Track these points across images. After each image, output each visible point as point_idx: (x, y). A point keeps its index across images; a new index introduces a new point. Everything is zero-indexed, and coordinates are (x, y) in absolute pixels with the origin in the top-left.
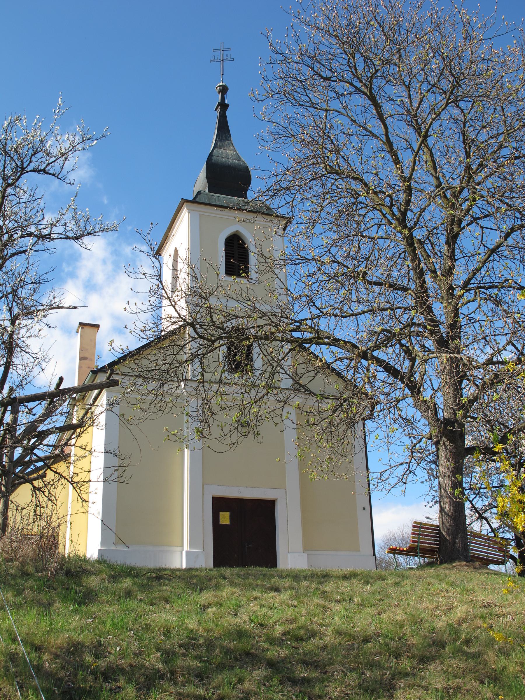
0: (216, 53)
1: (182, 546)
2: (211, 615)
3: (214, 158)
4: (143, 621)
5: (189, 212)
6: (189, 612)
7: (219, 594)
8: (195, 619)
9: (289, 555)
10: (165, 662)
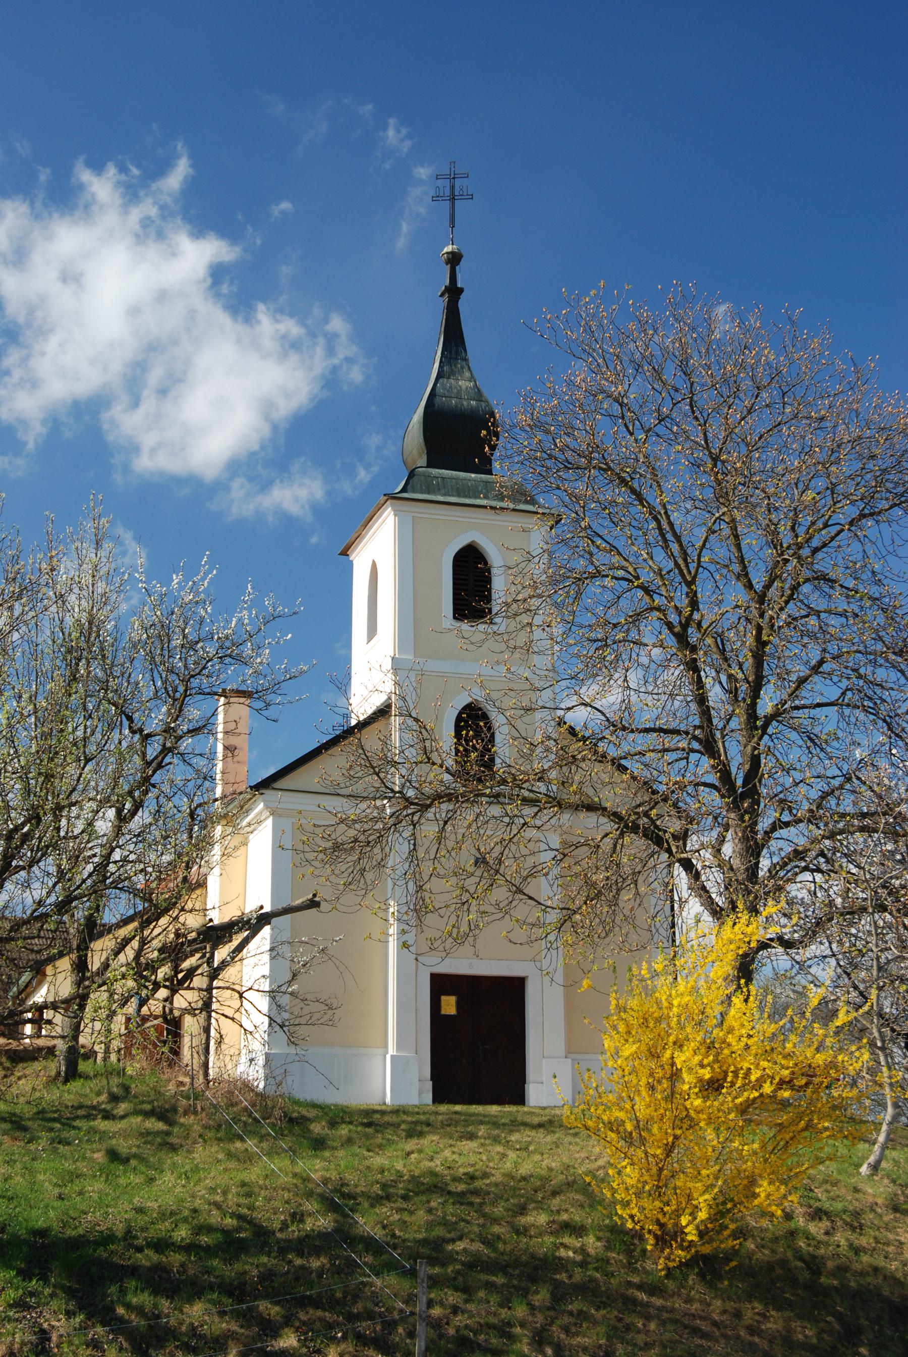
0: (440, 182)
1: (386, 1046)
2: (413, 1160)
3: (438, 401)
4: (366, 1163)
5: (395, 515)
6: (397, 1157)
7: (421, 1142)
8: (401, 1162)
9: (544, 1061)
10: (382, 1190)
